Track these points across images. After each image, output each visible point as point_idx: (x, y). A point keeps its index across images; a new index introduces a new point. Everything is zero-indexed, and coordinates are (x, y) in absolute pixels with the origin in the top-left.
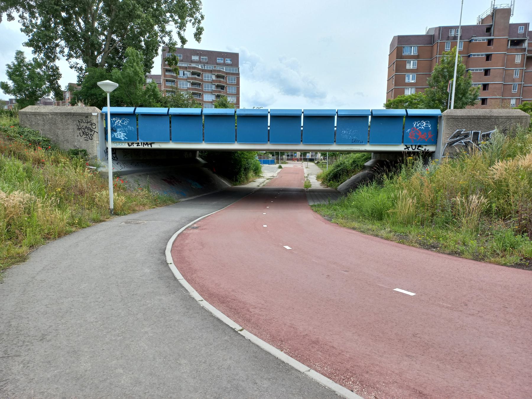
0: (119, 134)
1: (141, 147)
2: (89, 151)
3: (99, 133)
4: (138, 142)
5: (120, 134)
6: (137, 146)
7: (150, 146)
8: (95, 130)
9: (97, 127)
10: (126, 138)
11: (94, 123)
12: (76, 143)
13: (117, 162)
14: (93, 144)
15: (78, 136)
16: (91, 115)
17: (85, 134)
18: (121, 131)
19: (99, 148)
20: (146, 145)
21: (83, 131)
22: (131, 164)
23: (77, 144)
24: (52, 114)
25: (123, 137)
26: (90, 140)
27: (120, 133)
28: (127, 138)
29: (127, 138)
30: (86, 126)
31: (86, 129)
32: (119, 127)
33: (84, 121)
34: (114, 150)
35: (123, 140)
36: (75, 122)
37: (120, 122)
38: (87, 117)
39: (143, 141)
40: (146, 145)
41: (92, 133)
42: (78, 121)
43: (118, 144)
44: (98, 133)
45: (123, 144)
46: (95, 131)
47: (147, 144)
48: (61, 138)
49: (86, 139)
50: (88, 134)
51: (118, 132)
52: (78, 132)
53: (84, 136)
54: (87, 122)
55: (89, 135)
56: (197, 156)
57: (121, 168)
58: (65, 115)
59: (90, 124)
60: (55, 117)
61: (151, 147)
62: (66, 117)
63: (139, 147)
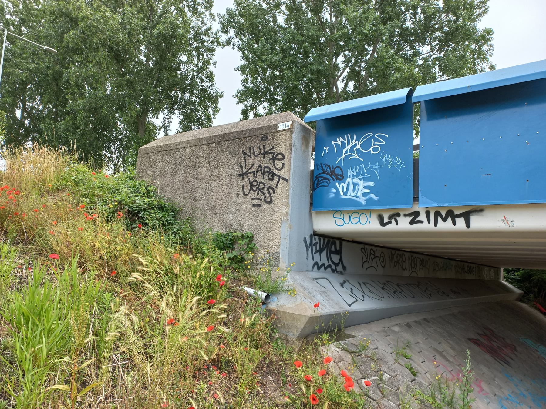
0: (351, 186)
1: (426, 226)
2: (260, 239)
3: (291, 182)
4: (416, 208)
5: (355, 185)
6: (412, 223)
7: (461, 223)
8: (281, 173)
9: (286, 165)
10: (372, 195)
11: (281, 154)
12: (231, 216)
13: (341, 279)
14: (273, 217)
15: (238, 195)
16: (273, 130)
17: (255, 188)
18: (356, 176)
19: (285, 231)
20: (445, 220)
21: (252, 179)
22: (383, 289)
23: (234, 220)
24: (192, 143)
25: (364, 195)
26: (265, 206)
27: (355, 181)
28: (376, 198)
29: (376, 198)
30: (260, 166)
31: (259, 174)
32: (354, 163)
33: (257, 151)
34: (338, 242)
35: (364, 203)
36: (236, 157)
37: (358, 146)
38: (264, 138)
39: (436, 205)
40: (445, 220)
41: (273, 184)
42: (243, 152)
43: (347, 219)
44: (287, 181)
45: (363, 219)
46: (280, 177)
47: (451, 214)
48: (202, 204)
49: (256, 202)
50: (262, 186)
51: (349, 180)
52: (241, 183)
53: (252, 195)
54: (265, 153)
55: (265, 191)
56: (501, 277)
57: (350, 300)
58: (217, 143)
59: (270, 156)
60: (195, 150)
61: (468, 225)
62: (217, 147)
63: (417, 227)
